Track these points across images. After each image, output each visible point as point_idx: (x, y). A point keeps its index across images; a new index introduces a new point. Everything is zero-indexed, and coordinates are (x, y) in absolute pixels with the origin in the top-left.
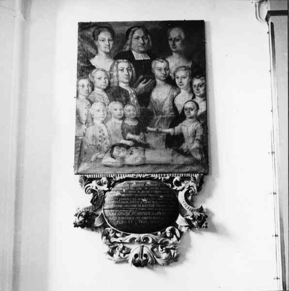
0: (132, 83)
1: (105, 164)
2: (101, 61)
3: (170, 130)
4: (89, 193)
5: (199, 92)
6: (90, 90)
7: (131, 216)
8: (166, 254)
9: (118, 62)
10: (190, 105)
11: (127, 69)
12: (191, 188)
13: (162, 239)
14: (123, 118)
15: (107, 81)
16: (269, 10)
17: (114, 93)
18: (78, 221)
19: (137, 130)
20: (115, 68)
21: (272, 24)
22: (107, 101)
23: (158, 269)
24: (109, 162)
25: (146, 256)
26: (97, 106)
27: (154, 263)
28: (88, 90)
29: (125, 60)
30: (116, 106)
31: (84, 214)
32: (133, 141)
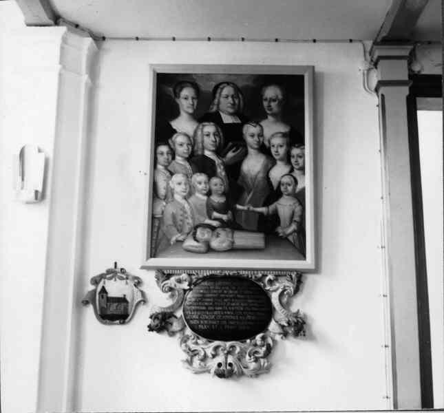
0: (220, 151)
1: (187, 248)
2: (183, 125)
3: (262, 210)
4: (166, 292)
5: (279, 155)
6: (170, 159)
7: (215, 319)
8: (254, 363)
9: (204, 126)
10: (287, 180)
11: (214, 135)
12: (287, 288)
13: (250, 349)
14: (209, 194)
15: (190, 148)
16: (380, 79)
17: (199, 163)
18: (153, 324)
19: (223, 209)
20: (199, 133)
21: (383, 95)
22: (190, 171)
23: (244, 380)
24: (192, 246)
25: (230, 365)
26: (179, 178)
27: (242, 374)
28: (168, 159)
29: (212, 123)
30: (200, 178)
31: (160, 316)
32: (220, 222)
